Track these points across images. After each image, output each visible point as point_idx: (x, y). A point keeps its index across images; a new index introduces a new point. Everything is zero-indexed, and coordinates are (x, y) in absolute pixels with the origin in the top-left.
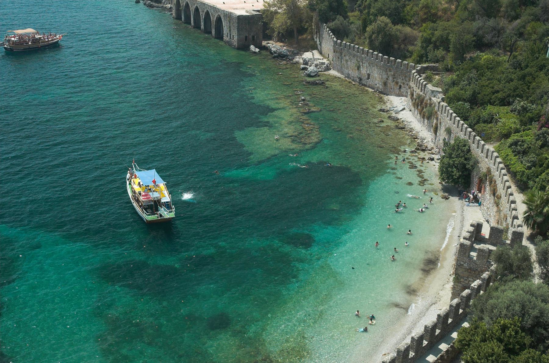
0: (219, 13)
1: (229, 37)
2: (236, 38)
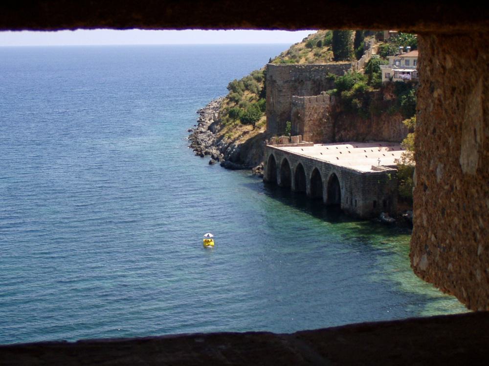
1: (349, 203)
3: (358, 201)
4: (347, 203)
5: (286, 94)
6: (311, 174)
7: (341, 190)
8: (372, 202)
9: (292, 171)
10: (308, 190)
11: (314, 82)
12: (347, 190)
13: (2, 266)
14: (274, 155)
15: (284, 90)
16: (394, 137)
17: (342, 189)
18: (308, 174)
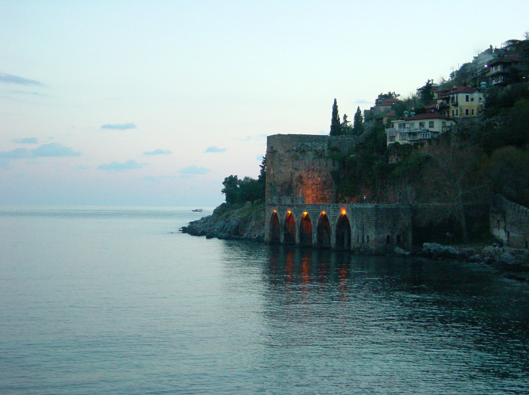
1: (360, 240)
3: (370, 236)
4: (358, 241)
5: (287, 164)
6: (317, 221)
7: (351, 229)
8: (386, 237)
9: (296, 223)
10: (315, 240)
11: (317, 152)
12: (358, 228)
13: (1, 351)
15: (286, 160)
16: (400, 199)
17: (352, 227)
18: (314, 223)
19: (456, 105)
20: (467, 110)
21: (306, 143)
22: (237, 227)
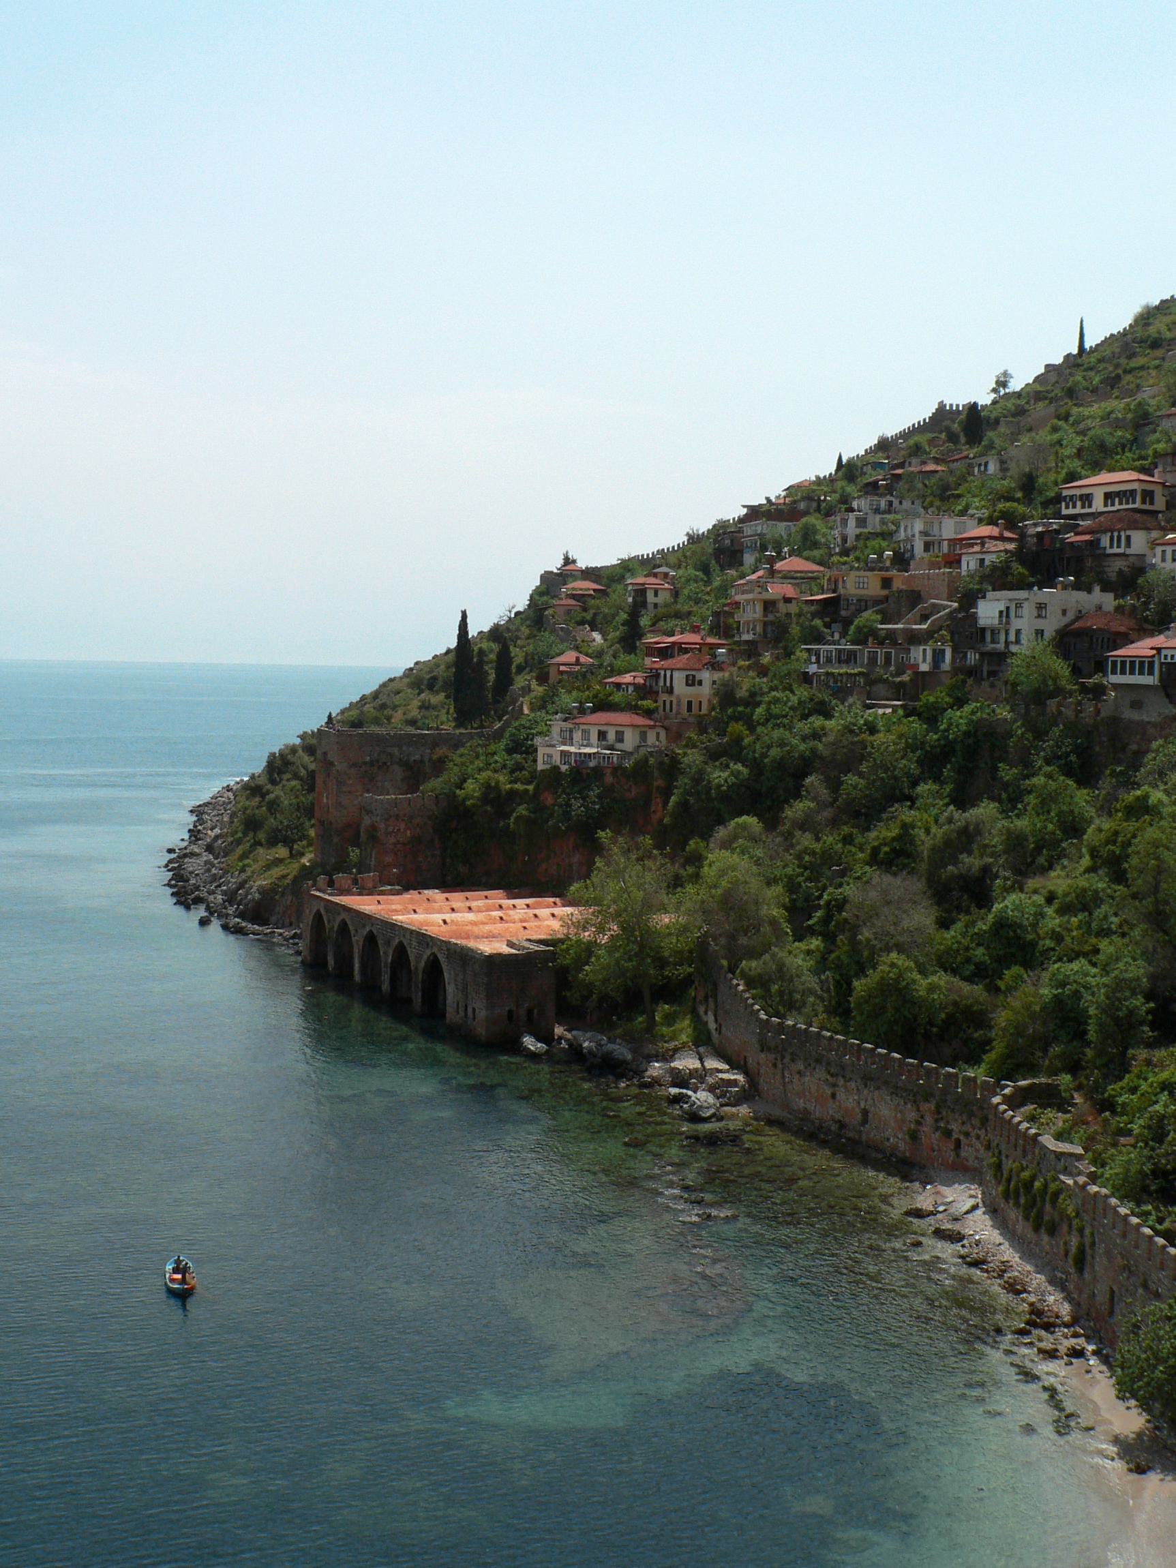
0: (435, 950)
1: (462, 1013)
2: (482, 1014)
6: (391, 952)
10: (386, 987)
14: (323, 912)
19: (670, 691)
20: (690, 703)
21: (389, 750)
22: (259, 904)
